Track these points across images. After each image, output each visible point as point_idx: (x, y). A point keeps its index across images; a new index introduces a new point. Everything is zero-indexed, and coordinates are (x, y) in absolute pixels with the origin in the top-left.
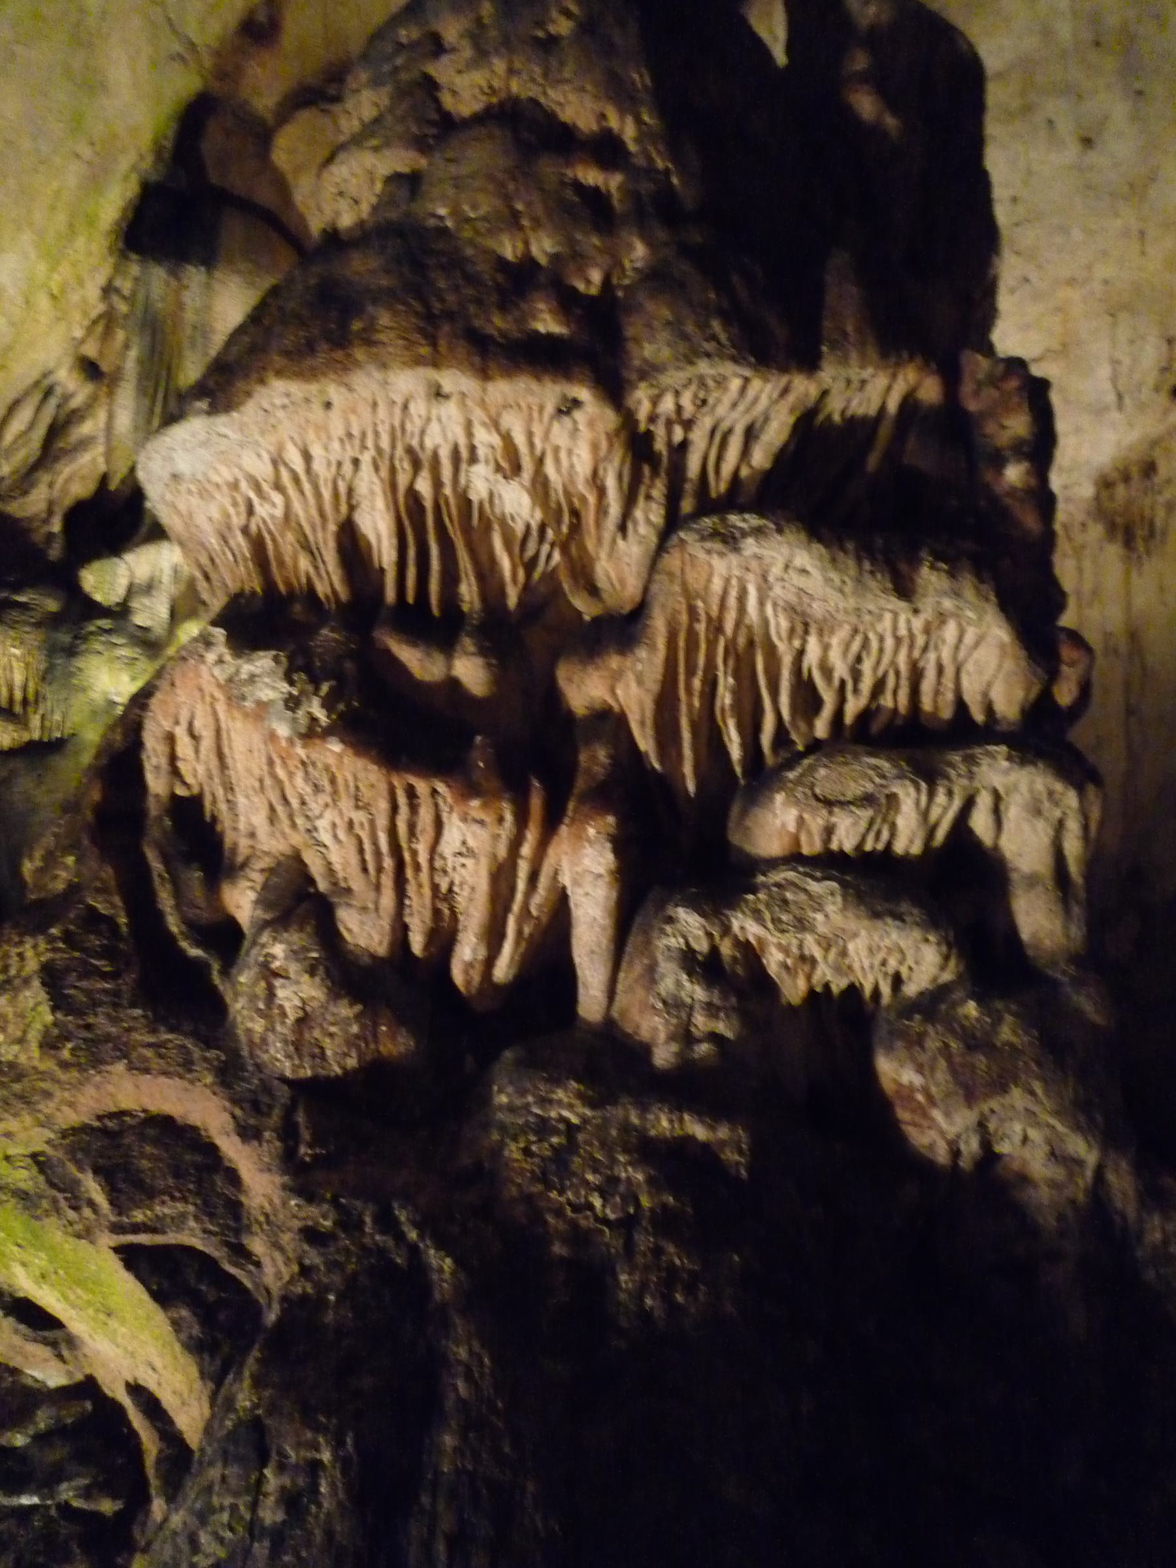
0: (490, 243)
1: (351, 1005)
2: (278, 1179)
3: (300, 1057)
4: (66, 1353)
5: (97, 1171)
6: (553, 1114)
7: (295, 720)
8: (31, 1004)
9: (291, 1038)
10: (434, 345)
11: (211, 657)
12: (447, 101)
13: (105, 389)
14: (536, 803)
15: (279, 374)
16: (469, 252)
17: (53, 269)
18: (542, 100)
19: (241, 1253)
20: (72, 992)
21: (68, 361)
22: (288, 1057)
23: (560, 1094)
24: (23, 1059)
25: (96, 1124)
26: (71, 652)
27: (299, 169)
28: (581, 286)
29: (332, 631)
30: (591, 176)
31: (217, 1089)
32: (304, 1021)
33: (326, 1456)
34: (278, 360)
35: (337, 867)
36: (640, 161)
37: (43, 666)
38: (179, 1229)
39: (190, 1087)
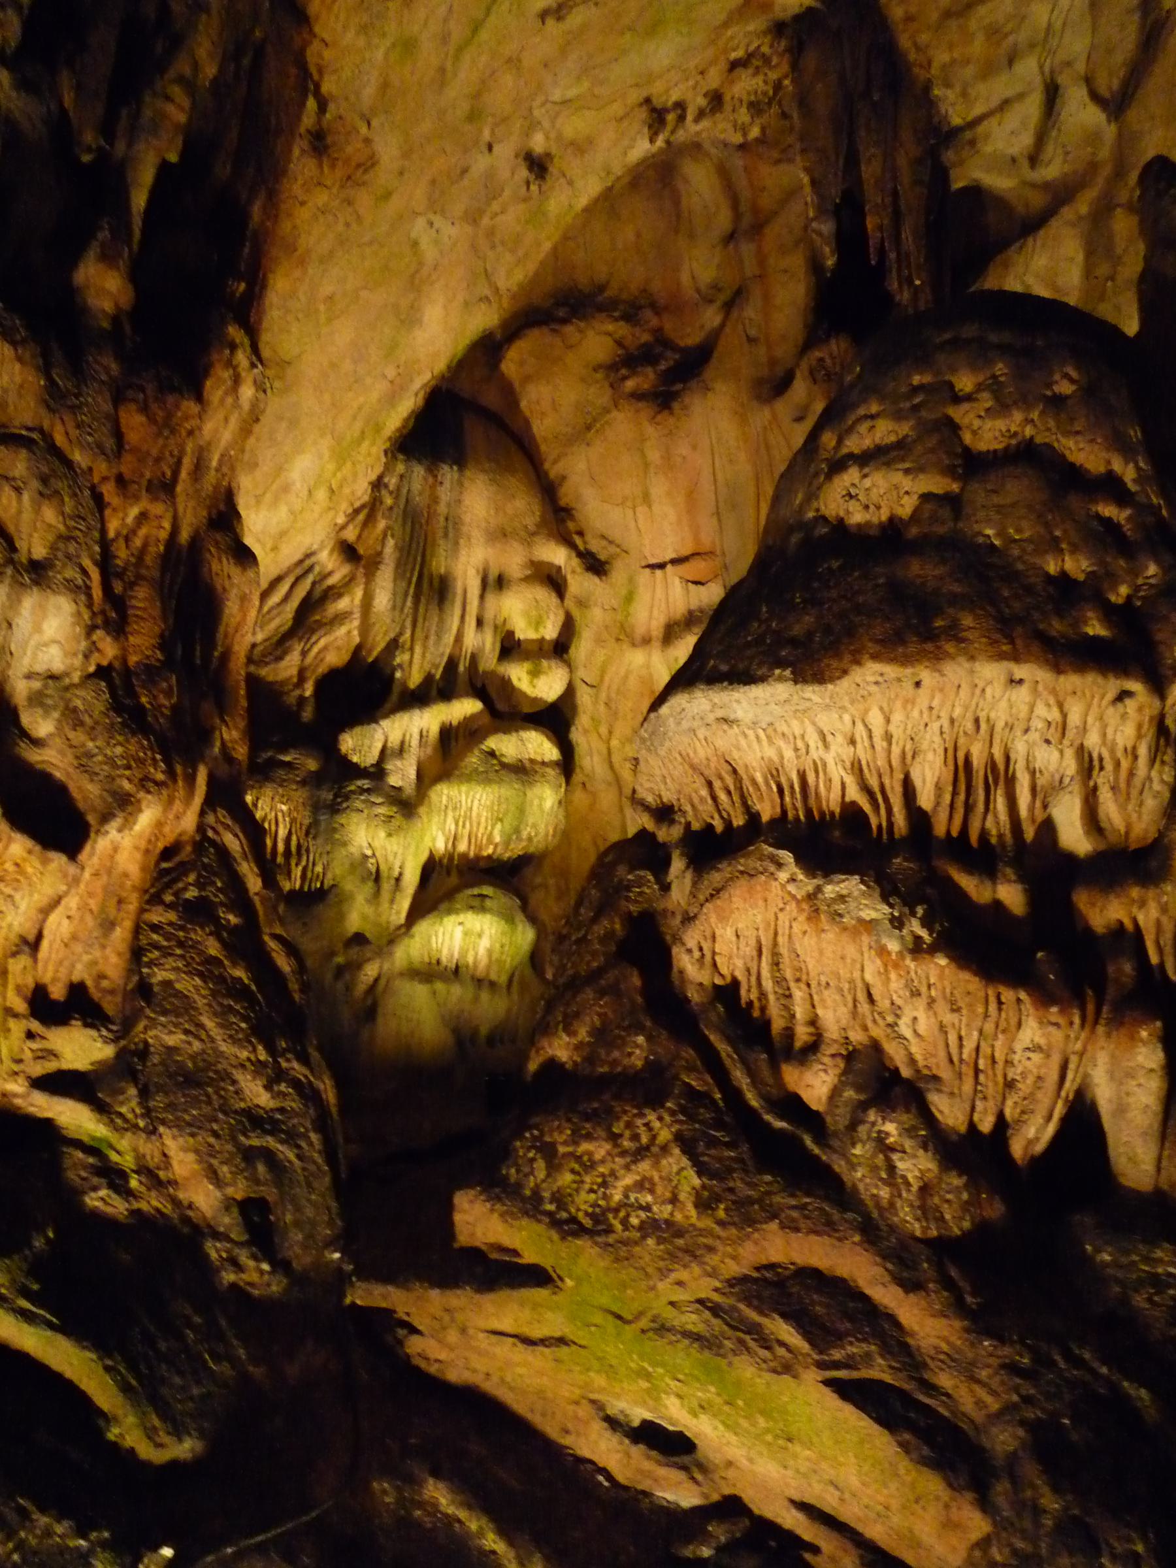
0: (1038, 561)
1: (960, 1176)
2: (957, 1324)
3: (927, 1219)
4: (699, 1477)
5: (785, 1316)
6: (1160, 1270)
7: (902, 937)
8: (675, 1169)
9: (917, 1203)
10: (1012, 642)
11: (783, 876)
12: (967, 438)
13: (361, 570)
14: (1091, 1008)
15: (875, 657)
16: (1020, 566)
17: (339, 469)
18: (1056, 445)
19: (931, 1388)
20: (706, 1159)
21: (330, 544)
22: (918, 1220)
23: (1159, 1254)
24: (678, 1217)
25: (755, 1275)
26: (334, 809)
27: (527, 379)
28: (1113, 598)
29: (906, 860)
30: (1108, 510)
31: (866, 1246)
32: (925, 1189)
33: (1140, 1548)
34: (872, 647)
35: (918, 1057)
36: (1142, 499)
37: (307, 822)
38: (870, 1366)
39: (837, 1243)
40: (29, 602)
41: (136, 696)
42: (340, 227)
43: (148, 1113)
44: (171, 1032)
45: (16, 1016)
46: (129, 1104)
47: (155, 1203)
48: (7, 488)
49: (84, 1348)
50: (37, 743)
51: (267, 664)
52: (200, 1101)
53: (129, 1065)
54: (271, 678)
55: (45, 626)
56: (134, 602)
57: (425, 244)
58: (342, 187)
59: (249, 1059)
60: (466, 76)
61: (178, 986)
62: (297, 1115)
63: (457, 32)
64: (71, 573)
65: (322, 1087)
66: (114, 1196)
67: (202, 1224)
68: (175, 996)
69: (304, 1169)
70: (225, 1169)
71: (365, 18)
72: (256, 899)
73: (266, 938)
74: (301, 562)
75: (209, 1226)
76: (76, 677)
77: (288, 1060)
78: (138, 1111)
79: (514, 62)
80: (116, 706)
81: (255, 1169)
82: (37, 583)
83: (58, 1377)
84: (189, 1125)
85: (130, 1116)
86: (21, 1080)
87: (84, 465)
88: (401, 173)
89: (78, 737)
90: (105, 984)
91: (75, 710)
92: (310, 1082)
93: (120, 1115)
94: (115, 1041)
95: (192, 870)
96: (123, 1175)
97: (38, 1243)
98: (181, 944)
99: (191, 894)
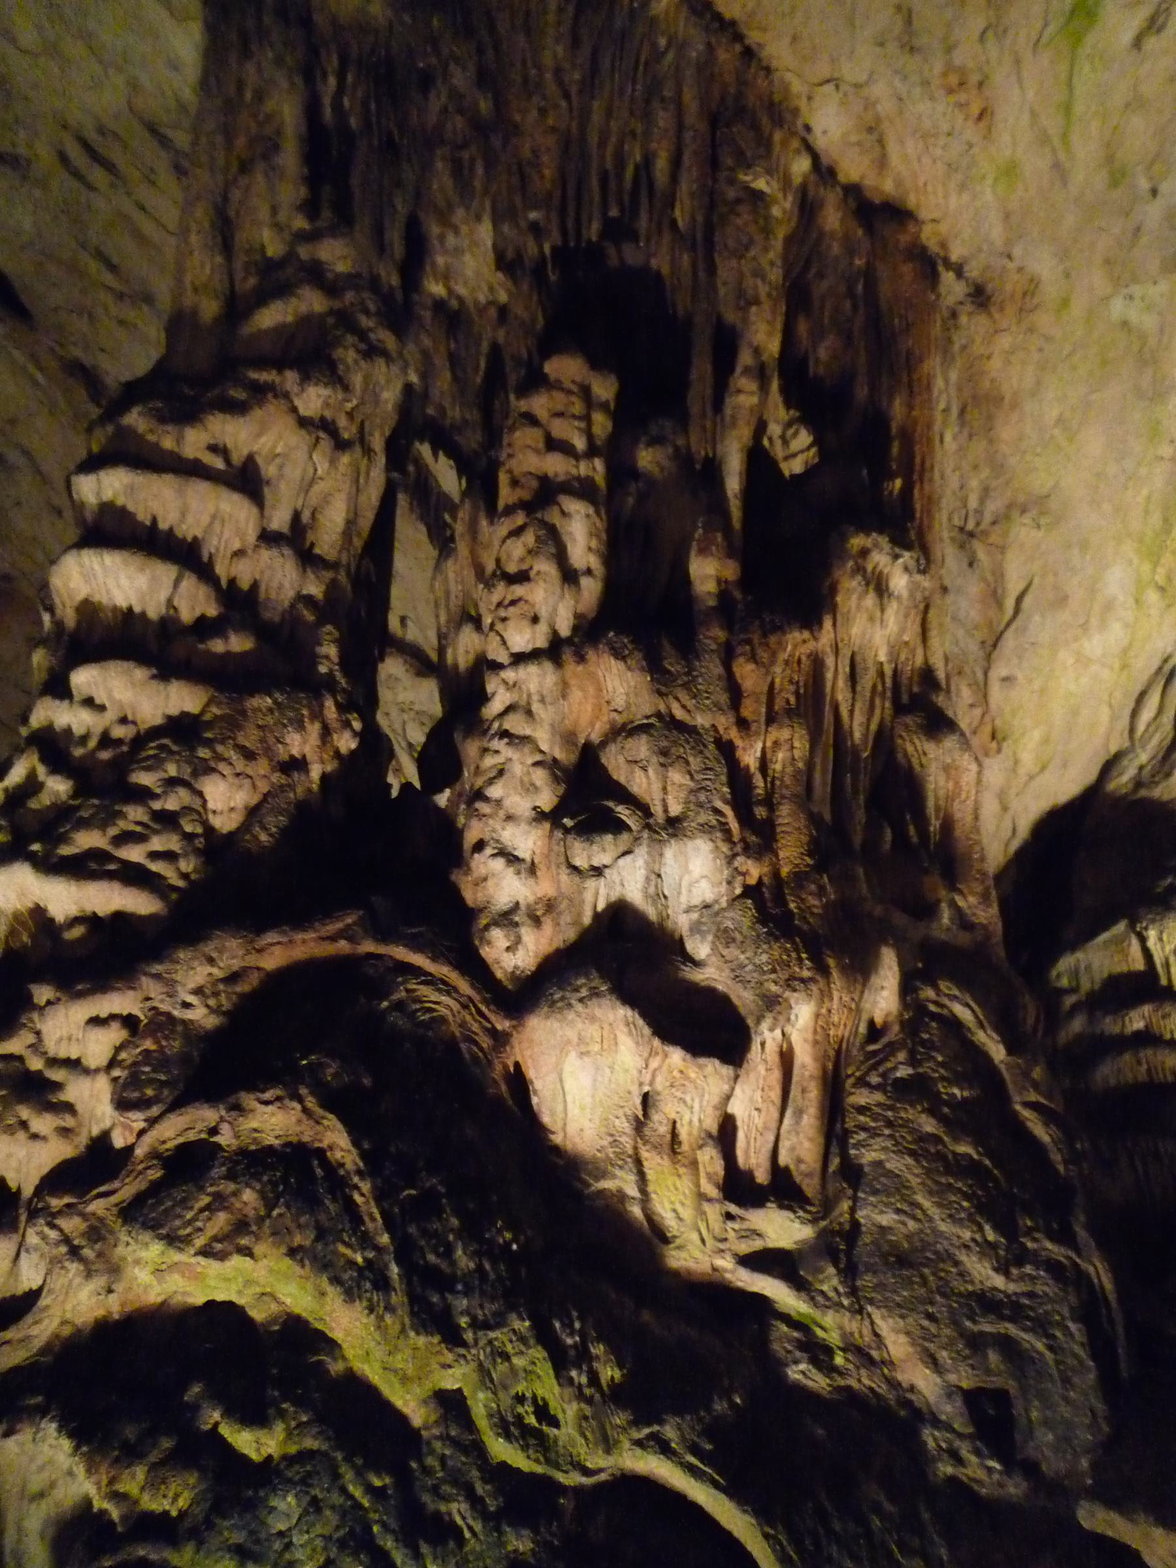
17: (1156, 564)
40: (671, 852)
41: (785, 904)
42: (1036, 356)
43: (853, 1292)
44: (882, 1212)
45: (709, 1200)
46: (830, 1281)
47: (866, 1382)
48: (637, 769)
49: (745, 1511)
50: (697, 964)
51: (1157, 784)
52: (913, 1283)
53: (839, 1246)
54: (1166, 797)
55: (691, 867)
56: (780, 821)
57: (1134, 316)
58: (1019, 322)
59: (974, 1240)
60: (1085, 151)
61: (888, 1166)
62: (1051, 1300)
63: (1052, 123)
64: (705, 817)
65: (1091, 1269)
66: (814, 1371)
67: (925, 1410)
68: (884, 1175)
69: (1058, 1363)
70: (945, 1354)
71: (959, 177)
72: (1002, 1068)
73: (1018, 1107)
74: (1160, 669)
75: (933, 1414)
76: (724, 903)
77: (1035, 1240)
78: (841, 1289)
79: (1136, 103)
80: (763, 917)
81: (985, 1357)
82: (674, 835)
83: (728, 1534)
84: (899, 1305)
85: (832, 1294)
86: (728, 1257)
87: (707, 725)
88: (1067, 275)
89: (732, 952)
90: (803, 1167)
91: (726, 930)
92: (1076, 1265)
93: (822, 1293)
94: (814, 1221)
95: (899, 1049)
96: (829, 1351)
97: (720, 1406)
98: (889, 1124)
99: (903, 1072)
